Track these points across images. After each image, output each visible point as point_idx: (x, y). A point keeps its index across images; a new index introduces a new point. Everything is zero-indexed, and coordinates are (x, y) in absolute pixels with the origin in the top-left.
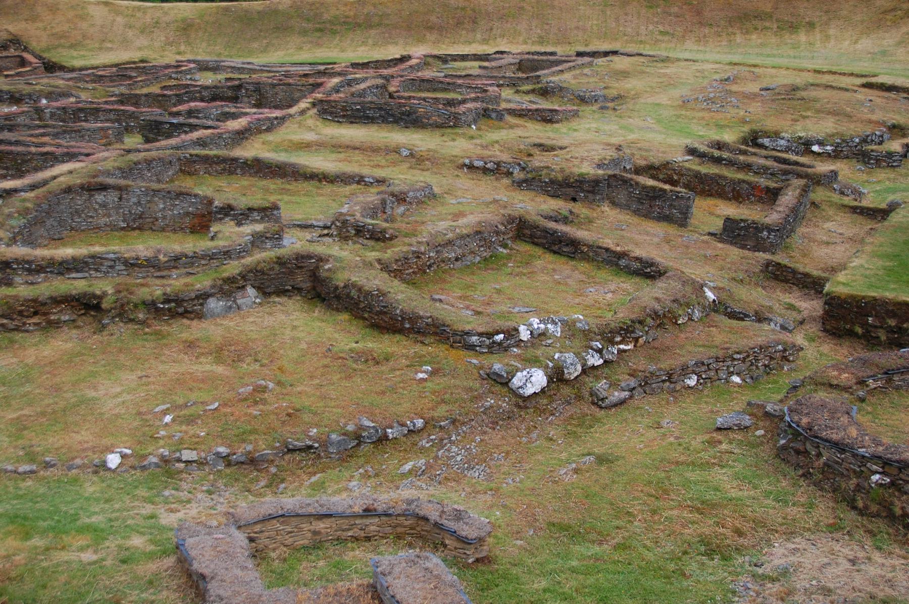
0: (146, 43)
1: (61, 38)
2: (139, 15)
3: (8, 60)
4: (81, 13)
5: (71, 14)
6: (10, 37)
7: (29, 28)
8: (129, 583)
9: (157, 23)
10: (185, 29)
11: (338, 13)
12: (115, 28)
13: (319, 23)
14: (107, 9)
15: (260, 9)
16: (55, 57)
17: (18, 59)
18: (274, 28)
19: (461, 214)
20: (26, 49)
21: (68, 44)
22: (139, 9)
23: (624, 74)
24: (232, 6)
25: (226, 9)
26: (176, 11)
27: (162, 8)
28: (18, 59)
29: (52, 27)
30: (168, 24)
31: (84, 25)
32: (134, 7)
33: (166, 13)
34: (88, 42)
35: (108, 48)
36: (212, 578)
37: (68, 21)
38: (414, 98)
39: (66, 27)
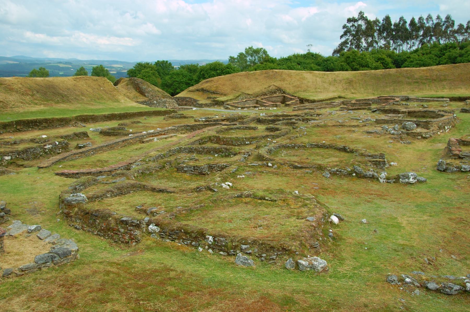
0: (335, 89)
1: (298, 87)
2: (325, 77)
3: (278, 98)
4: (301, 77)
5: (298, 77)
6: (277, 88)
7: (283, 84)
8: (58, 239)
9: (335, 80)
10: (349, 83)
11: (421, 75)
12: (318, 83)
13: (414, 79)
14: (311, 75)
15: (381, 73)
16: (303, 95)
17: (282, 97)
18: (392, 82)
19: (302, 152)
20: (284, 92)
21: (302, 90)
22: (325, 74)
23: (169, 125)
24: (367, 72)
25: (365, 74)
26: (342, 75)
27: (335, 74)
28: (282, 97)
29: (292, 83)
30: (341, 81)
31: (305, 82)
32: (322, 74)
33: (337, 76)
34: (309, 89)
35: (319, 92)
36: (8, 253)
37: (298, 80)
38: (22, 141)
39: (298, 83)
